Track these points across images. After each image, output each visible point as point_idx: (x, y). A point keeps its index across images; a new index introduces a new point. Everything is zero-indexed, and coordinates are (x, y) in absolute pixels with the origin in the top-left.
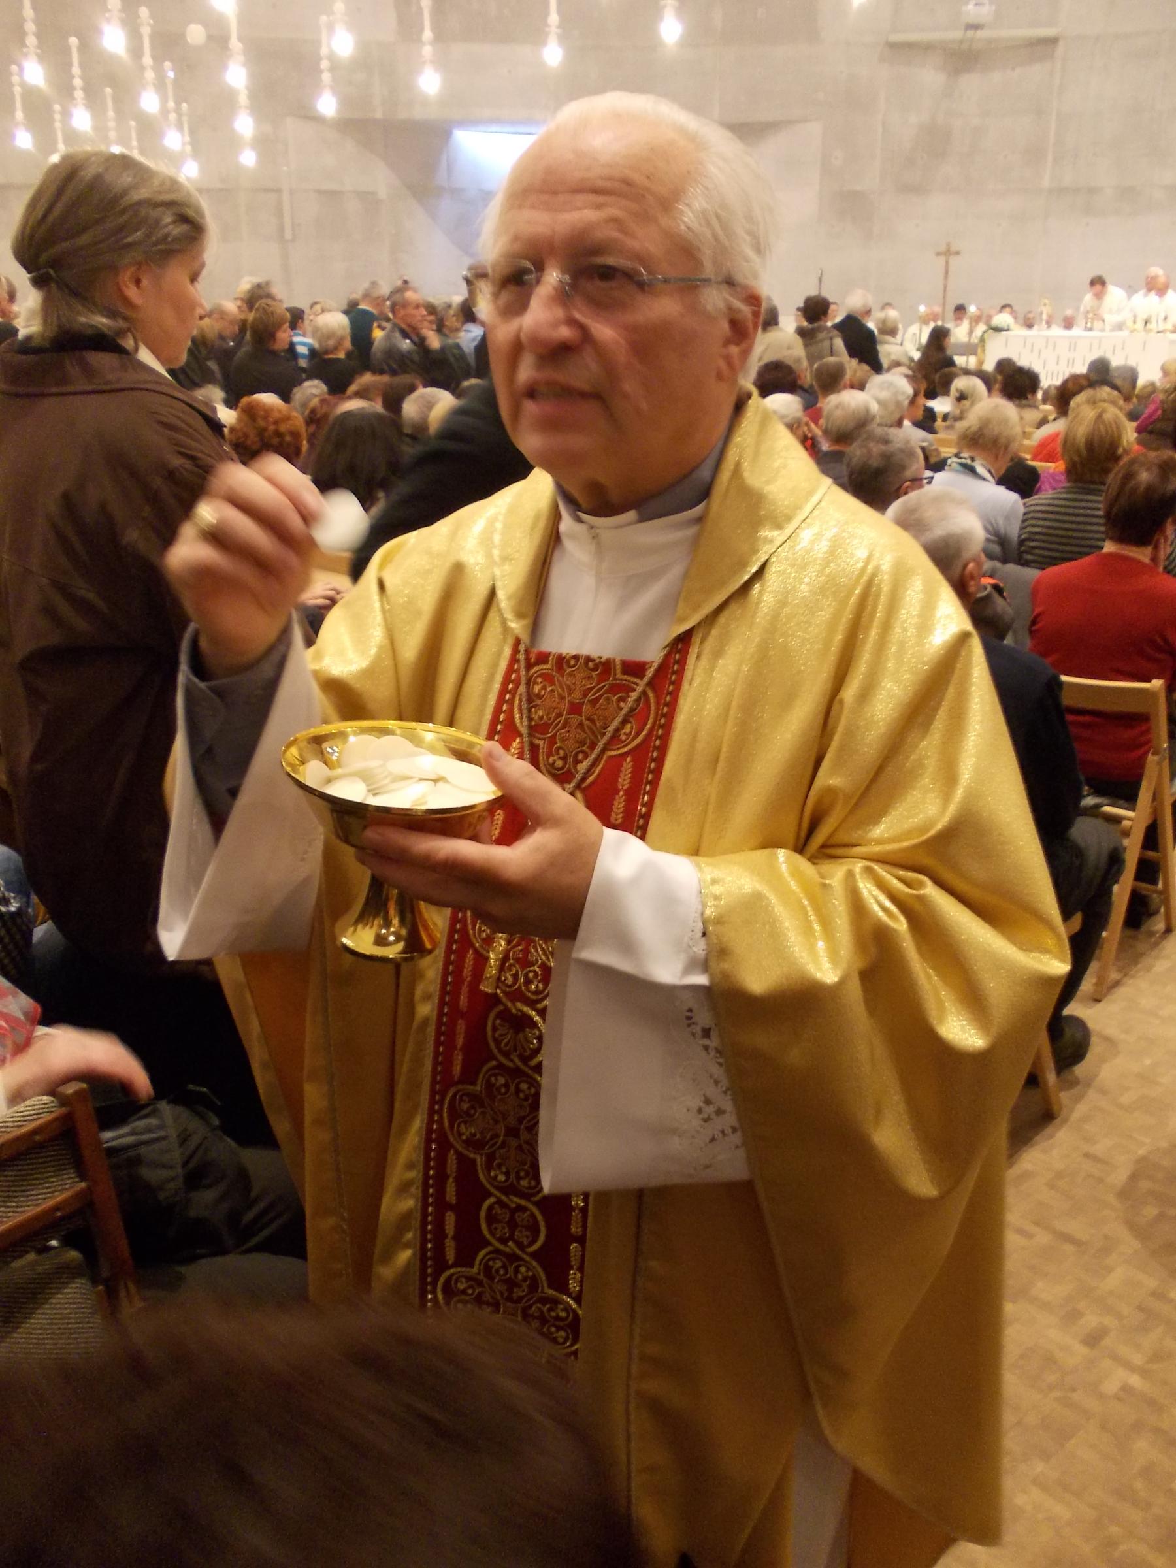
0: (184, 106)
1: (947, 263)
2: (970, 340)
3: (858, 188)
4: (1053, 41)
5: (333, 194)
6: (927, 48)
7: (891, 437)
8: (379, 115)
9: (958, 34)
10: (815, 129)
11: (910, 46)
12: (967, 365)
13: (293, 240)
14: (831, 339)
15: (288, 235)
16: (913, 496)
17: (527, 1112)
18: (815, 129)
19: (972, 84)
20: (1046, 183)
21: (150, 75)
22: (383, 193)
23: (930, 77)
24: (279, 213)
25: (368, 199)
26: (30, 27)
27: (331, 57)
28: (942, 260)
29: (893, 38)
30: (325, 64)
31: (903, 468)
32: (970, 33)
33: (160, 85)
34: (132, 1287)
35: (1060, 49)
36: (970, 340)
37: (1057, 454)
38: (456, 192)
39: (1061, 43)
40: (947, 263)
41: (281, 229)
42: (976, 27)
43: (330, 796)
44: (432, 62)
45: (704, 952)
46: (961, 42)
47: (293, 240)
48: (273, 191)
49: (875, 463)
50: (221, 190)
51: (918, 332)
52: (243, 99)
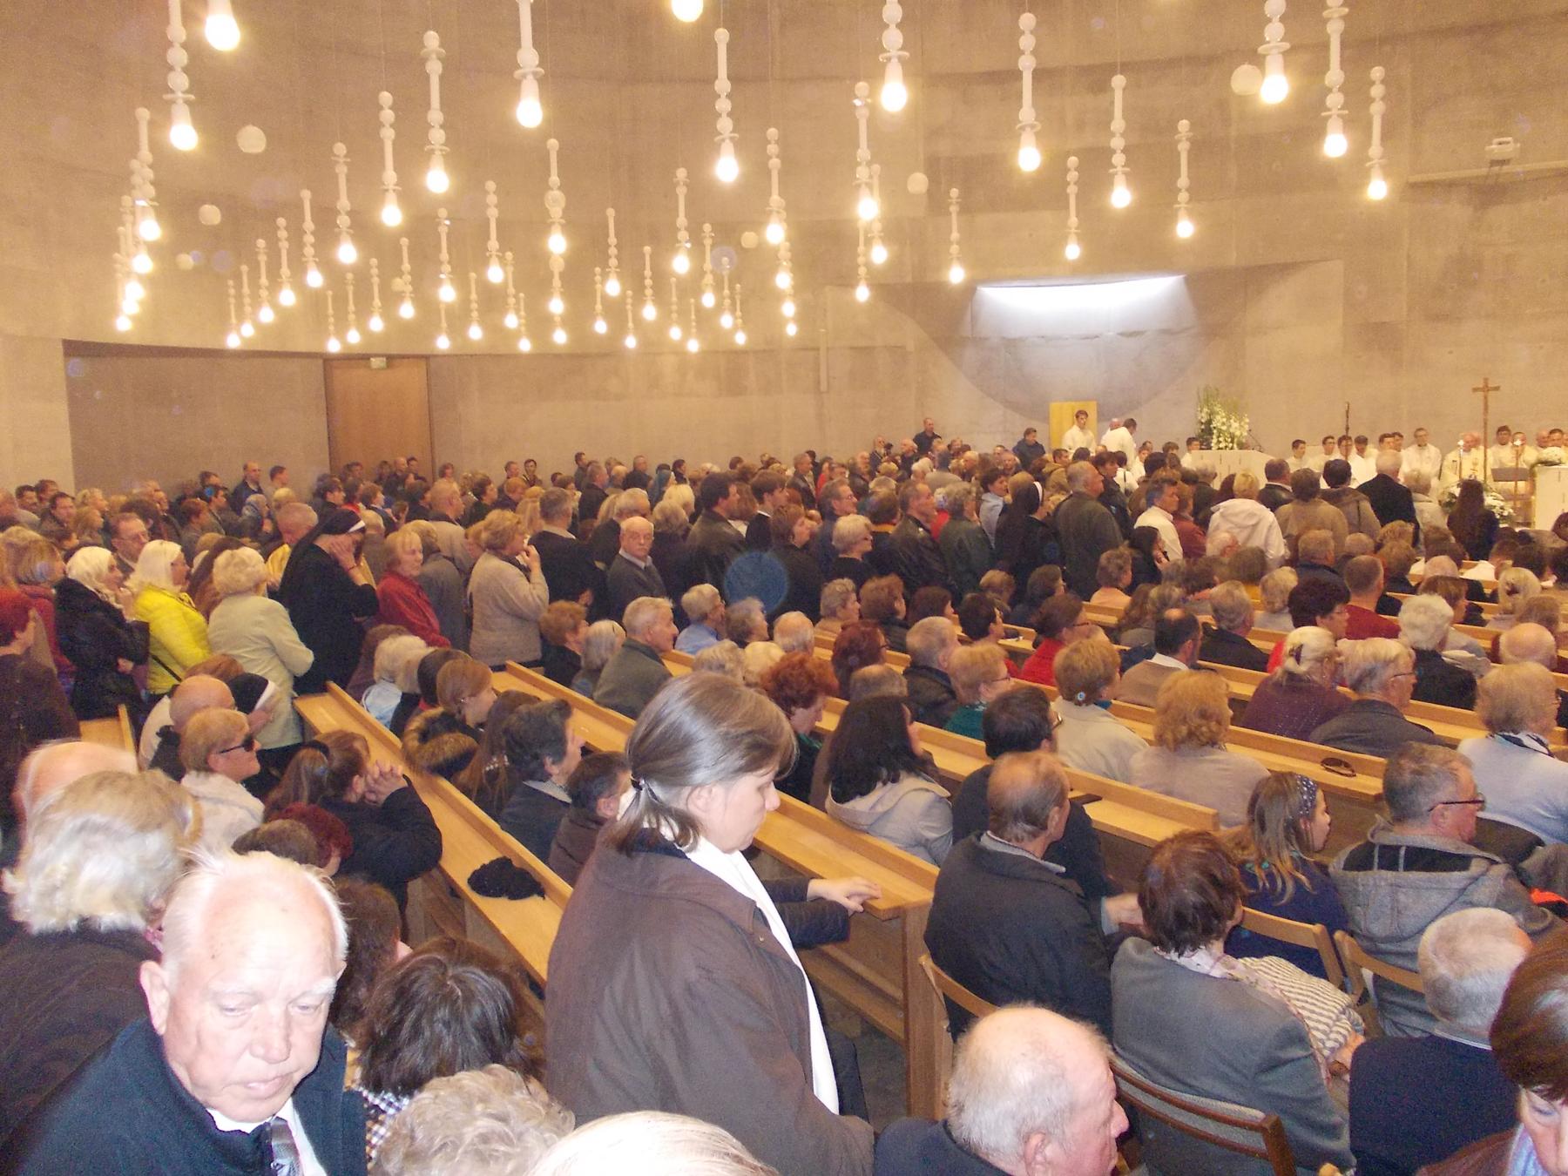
1: (1486, 398)
2: (1517, 464)
3: (1386, 319)
5: (867, 351)
6: (1451, 185)
8: (909, 279)
9: (1484, 171)
10: (1337, 267)
11: (1432, 184)
12: (1516, 491)
14: (1358, 502)
15: (823, 387)
17: (1056, 545)
18: (1337, 267)
19: (1501, 215)
21: (1335, 100)
22: (911, 346)
23: (1457, 211)
25: (898, 352)
26: (613, 251)
27: (868, 265)
28: (1480, 394)
29: (1413, 179)
30: (862, 271)
32: (1496, 169)
33: (1356, 122)
34: (530, 599)
36: (1517, 464)
38: (979, 341)
40: (1486, 398)
42: (1503, 162)
44: (958, 258)
45: (1269, 774)
46: (1487, 177)
48: (813, 349)
50: (764, 351)
51: (1458, 459)
52: (784, 253)
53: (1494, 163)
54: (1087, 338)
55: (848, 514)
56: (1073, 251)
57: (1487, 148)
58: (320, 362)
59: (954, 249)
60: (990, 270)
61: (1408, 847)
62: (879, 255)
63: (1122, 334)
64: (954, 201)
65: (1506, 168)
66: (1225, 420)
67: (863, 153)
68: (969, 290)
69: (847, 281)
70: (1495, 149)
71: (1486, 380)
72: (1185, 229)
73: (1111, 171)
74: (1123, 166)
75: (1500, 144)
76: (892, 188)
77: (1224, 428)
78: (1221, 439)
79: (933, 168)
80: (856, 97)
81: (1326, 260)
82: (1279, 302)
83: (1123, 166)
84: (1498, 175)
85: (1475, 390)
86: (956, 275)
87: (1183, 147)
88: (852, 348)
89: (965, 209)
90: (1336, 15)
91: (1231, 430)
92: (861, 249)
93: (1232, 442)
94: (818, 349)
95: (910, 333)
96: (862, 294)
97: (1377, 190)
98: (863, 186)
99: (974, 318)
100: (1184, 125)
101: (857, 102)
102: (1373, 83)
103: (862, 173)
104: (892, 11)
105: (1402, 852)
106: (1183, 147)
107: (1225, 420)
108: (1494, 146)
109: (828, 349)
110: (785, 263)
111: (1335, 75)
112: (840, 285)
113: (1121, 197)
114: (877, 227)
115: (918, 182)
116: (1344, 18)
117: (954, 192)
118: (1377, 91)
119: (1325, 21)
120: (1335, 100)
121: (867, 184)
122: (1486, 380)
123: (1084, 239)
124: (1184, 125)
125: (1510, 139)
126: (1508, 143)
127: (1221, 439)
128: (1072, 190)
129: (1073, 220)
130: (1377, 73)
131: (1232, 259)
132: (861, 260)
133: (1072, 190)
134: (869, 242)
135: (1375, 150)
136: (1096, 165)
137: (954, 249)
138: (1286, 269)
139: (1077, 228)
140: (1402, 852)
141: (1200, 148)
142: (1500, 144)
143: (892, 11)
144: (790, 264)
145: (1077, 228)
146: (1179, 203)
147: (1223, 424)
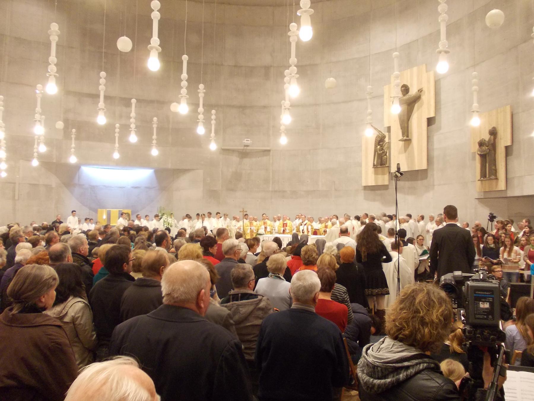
0: (397, 236)
4: (269, 151)
6: (233, 151)
7: (245, 267)
8: (54, 161)
9: (242, 148)
10: (201, 172)
13: (18, 200)
15: (16, 198)
16: (23, 267)
18: (201, 172)
19: (246, 161)
20: (271, 189)
21: (201, 117)
22: (54, 185)
23: (235, 159)
24: (14, 191)
25: (48, 188)
29: (223, 148)
31: (250, 277)
32: (246, 148)
33: (207, 122)
35: (271, 152)
37: (330, 274)
38: (81, 186)
39: (271, 151)
41: (14, 196)
42: (247, 146)
43: (530, 372)
46: (243, 150)
47: (18, 200)
49: (242, 276)
53: (245, 146)
54: (121, 188)
55: (23, 242)
56: (116, 155)
57: (243, 141)
58: (424, 166)
59: (73, 150)
60: (86, 160)
61: (241, 293)
62: (43, 149)
63: (132, 187)
64: (74, 133)
65: (248, 148)
66: (166, 217)
67: (38, 109)
68: (77, 168)
69: (29, 158)
70: (245, 142)
71: (243, 209)
72: (155, 152)
73: (130, 129)
74: (134, 129)
75: (247, 140)
76: (49, 124)
77: (166, 220)
78: (165, 224)
79: (66, 121)
80: (37, 89)
81: (197, 169)
82: (184, 181)
83: (134, 129)
84: (246, 149)
85: (240, 212)
86: (73, 160)
87: (155, 126)
88: (30, 184)
89: (77, 139)
90: (202, 92)
91: (168, 221)
92: (36, 146)
93: (168, 225)
94: (15, 183)
95: (54, 181)
96: (35, 163)
97: (213, 147)
98: (38, 121)
99: (79, 178)
100: (155, 119)
101: (38, 92)
102: (212, 120)
103: (37, 116)
104: (56, 1)
105: (240, 295)
106: (155, 126)
107: (166, 217)
108: (245, 141)
109: (19, 184)
110: (3, 148)
111: (201, 109)
112: (26, 160)
113: (133, 138)
114: (42, 138)
115: (60, 125)
116: (204, 93)
117: (74, 130)
118: (213, 117)
119: (199, 93)
120: (201, 117)
121: (39, 121)
122: (243, 209)
123: (121, 152)
124: (155, 119)
125: (249, 140)
126: (249, 141)
127: (165, 224)
128: (117, 135)
129: (117, 145)
130: (213, 112)
131: (169, 166)
132: (35, 150)
133: (117, 135)
134: (38, 144)
135: (213, 134)
136: (125, 129)
137: (73, 150)
138: (185, 171)
139: (118, 148)
140: (240, 295)
141: (159, 129)
142: (247, 140)
143: (56, 1)
144: (5, 149)
145: (118, 148)
146: (153, 144)
147: (166, 219)
